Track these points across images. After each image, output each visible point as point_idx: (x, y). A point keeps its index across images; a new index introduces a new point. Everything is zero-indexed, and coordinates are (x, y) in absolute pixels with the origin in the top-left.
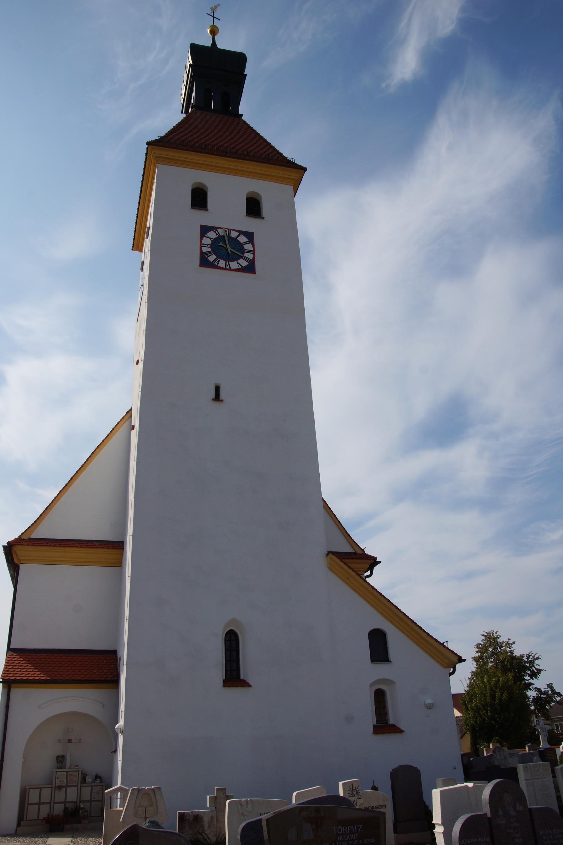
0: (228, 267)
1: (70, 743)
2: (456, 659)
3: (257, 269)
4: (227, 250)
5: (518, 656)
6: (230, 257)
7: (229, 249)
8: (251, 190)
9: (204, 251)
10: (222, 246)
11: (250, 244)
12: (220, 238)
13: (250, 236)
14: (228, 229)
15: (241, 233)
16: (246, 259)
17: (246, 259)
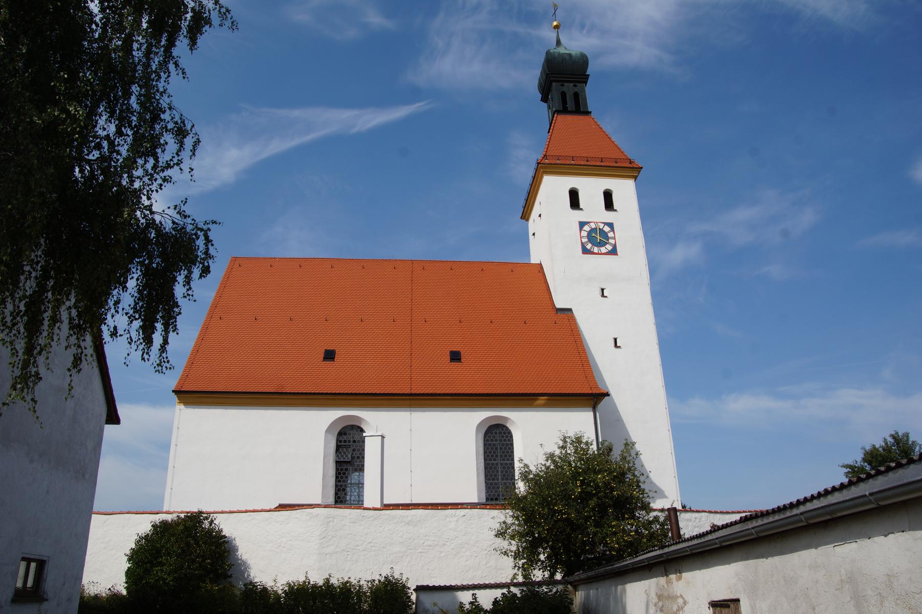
5: (491, 607)
6: (601, 244)
12: (593, 230)
13: (611, 225)
15: (605, 224)
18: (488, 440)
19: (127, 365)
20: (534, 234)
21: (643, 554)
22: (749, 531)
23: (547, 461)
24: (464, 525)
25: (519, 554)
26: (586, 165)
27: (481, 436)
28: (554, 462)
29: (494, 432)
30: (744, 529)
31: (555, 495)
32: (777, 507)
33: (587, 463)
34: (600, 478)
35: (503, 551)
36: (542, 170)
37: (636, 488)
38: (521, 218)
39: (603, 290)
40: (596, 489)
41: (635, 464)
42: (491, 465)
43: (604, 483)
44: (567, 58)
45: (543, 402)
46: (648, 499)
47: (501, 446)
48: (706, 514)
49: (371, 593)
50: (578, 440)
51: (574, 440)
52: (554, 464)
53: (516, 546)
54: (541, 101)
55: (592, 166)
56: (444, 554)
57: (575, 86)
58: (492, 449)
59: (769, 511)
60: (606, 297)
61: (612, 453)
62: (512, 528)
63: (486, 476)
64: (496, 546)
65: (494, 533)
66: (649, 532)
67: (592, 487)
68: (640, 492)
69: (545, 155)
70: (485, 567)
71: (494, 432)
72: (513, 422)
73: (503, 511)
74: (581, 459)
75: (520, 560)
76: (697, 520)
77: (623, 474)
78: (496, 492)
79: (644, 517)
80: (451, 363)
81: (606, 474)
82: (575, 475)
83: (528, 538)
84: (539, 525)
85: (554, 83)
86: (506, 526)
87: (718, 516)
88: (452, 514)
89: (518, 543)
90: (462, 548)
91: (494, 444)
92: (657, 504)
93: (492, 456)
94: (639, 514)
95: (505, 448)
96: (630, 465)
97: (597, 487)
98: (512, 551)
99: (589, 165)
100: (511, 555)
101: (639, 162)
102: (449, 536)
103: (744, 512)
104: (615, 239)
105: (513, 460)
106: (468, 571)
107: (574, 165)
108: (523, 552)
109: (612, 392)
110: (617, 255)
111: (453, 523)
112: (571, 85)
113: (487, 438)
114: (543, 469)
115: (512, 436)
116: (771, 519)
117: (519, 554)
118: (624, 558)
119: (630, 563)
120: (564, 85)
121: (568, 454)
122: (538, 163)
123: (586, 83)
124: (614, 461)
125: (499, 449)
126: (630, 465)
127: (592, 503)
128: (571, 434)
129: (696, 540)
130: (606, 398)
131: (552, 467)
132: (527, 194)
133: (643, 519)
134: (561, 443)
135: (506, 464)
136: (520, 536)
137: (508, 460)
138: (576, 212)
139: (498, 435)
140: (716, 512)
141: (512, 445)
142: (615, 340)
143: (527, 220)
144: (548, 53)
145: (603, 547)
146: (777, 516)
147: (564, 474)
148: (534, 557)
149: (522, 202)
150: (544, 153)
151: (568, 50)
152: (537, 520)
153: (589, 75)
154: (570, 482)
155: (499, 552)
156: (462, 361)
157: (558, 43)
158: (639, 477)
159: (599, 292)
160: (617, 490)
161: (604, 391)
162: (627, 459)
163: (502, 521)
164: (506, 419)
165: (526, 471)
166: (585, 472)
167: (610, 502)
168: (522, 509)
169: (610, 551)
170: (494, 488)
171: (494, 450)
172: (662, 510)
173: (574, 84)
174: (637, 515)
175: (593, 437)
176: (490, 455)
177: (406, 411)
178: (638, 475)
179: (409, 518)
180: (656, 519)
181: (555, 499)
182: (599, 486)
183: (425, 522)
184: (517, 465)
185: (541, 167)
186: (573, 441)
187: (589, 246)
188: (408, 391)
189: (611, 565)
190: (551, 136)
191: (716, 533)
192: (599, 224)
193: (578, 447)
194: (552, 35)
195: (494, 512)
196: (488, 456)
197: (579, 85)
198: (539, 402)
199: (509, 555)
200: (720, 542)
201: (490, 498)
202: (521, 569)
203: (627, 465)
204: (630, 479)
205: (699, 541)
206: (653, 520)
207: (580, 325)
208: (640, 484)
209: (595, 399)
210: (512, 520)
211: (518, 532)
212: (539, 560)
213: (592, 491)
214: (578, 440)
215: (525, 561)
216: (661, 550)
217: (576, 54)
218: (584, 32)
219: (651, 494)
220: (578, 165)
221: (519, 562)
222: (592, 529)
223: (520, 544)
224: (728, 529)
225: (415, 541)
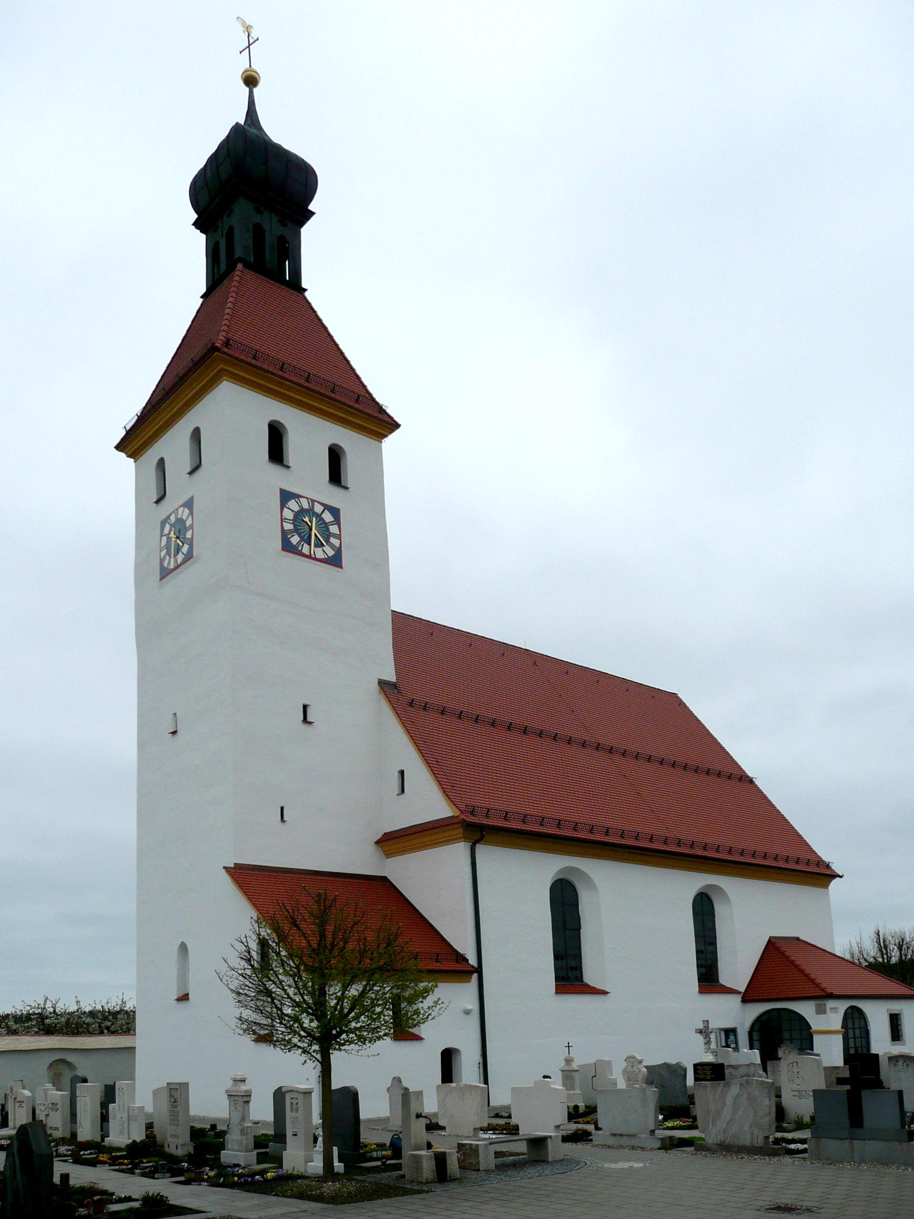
0: (313, 556)
1: (497, 1150)
2: (770, 944)
3: (344, 563)
4: (311, 529)
7: (314, 531)
8: (332, 442)
9: (285, 529)
10: (306, 522)
11: (336, 526)
14: (312, 500)
15: (327, 507)
16: (332, 546)
17: (332, 546)
19: (76, 997)
49: (352, 998)
110: (341, 567)
138: (275, 469)
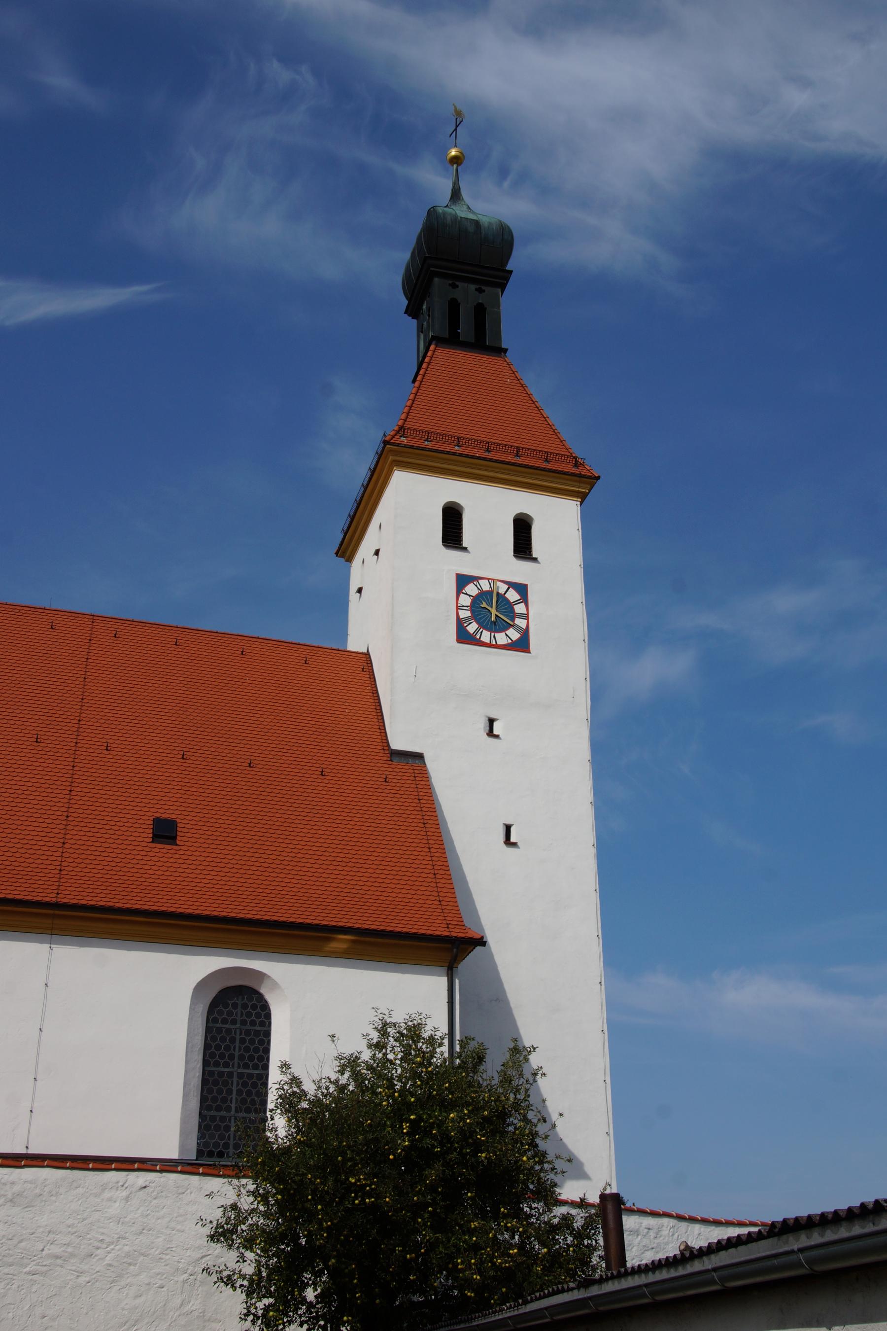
6: (498, 626)
12: (484, 596)
13: (522, 589)
15: (511, 585)
16: (518, 628)
17: (518, 628)
18: (215, 1020)
20: (360, 591)
21: (541, 1298)
22: (793, 1257)
23: (343, 1074)
24: (142, 1209)
25: (258, 1285)
26: (485, 459)
27: (202, 1009)
28: (356, 1076)
29: (230, 1002)
30: (781, 1250)
31: (353, 1151)
32: (858, 1205)
33: (427, 1083)
34: (453, 1118)
35: (225, 1274)
36: (391, 458)
37: (529, 1150)
38: (337, 554)
39: (491, 721)
40: (442, 1145)
41: (529, 1096)
42: (216, 1077)
43: (461, 1131)
44: (471, 229)
45: (344, 946)
46: (551, 1176)
47: (243, 1036)
48: (672, 1222)
50: (414, 1032)
51: (405, 1032)
52: (355, 1081)
53: (254, 1265)
54: (405, 313)
55: (496, 461)
56: (87, 1279)
57: (480, 291)
58: (223, 1039)
59: (855, 1211)
60: (497, 737)
61: (482, 1068)
62: (250, 1221)
63: (203, 1099)
64: (209, 1261)
65: (207, 1230)
66: (549, 1251)
67: (434, 1137)
68: (537, 1159)
69: (402, 428)
70: (177, 1313)
71: (230, 1002)
72: (275, 985)
73: (235, 1181)
74: (415, 1075)
75: (260, 1299)
76: (652, 1234)
77: (503, 1115)
78: (222, 1137)
79: (540, 1214)
80: (153, 845)
81: (466, 1112)
82: (400, 1110)
83: (283, 1247)
84: (311, 1216)
85: (436, 280)
86: (238, 1216)
87: (697, 1228)
88: (118, 1182)
89: (260, 1256)
90: (130, 1264)
91: (228, 1031)
92: (570, 1190)
93: (222, 1056)
94: (531, 1208)
95: (252, 1042)
96: (518, 1096)
97: (445, 1139)
98: (243, 1277)
99: (491, 460)
100: (241, 1286)
101: (593, 466)
102: (103, 1234)
103: (753, 1224)
104: (528, 619)
105: (266, 1067)
106: (137, 1321)
107: (461, 455)
108: (269, 1279)
109: (490, 938)
110: (529, 652)
111: (117, 1204)
112: (472, 287)
113: (215, 1015)
114: (331, 1090)
115: (268, 1016)
116: (843, 1232)
117: (258, 1285)
118: (491, 1307)
119: (509, 1318)
120: (457, 286)
121: (388, 1060)
122: (386, 443)
123: (503, 287)
124: (485, 1084)
125: (237, 1041)
126: (518, 1096)
127: (432, 1174)
128: (399, 1017)
129: (664, 1271)
130: (479, 949)
131: (351, 1088)
132: (356, 505)
133: (537, 1219)
134: (375, 1036)
135: (250, 1076)
136: (265, 1242)
137: (256, 1067)
139: (239, 1009)
140: (692, 1220)
141: (268, 1034)
142: (508, 828)
143: (350, 559)
144: (432, 213)
145: (447, 1279)
146: (857, 1227)
147: (377, 1105)
148: (292, 1293)
149: (342, 522)
150: (400, 423)
151: (474, 213)
152: (308, 1205)
153: (511, 272)
154: (388, 1123)
155: (214, 1278)
156: (178, 842)
157: (456, 195)
158: (536, 1126)
159: (483, 725)
160: (488, 1151)
161: (474, 933)
162: (515, 1083)
163: (229, 1202)
164: (261, 976)
165: (294, 1093)
166: (424, 1102)
167: (470, 1175)
168: (278, 1179)
169: (461, 1289)
170: (218, 1128)
171: (228, 1042)
172: (582, 1204)
173: (477, 287)
174: (526, 1209)
175: (444, 1029)
176: (217, 1053)
177: (41, 942)
178: (535, 1121)
179: (17, 1188)
180: (567, 1220)
181: (350, 1159)
182: (449, 1138)
183: (54, 1198)
184: (275, 1076)
185: (391, 450)
186: (402, 1035)
187: (472, 628)
188: (50, 898)
189: (465, 1321)
190: (419, 388)
191: (713, 1256)
192: (499, 584)
193: (410, 1046)
194: (445, 186)
195: (215, 1184)
196: (212, 1055)
197: (488, 290)
198: (334, 945)
199: (238, 1285)
200: (723, 1279)
201: (206, 1150)
202: (259, 1322)
203: (512, 1096)
204: (516, 1129)
205: (673, 1273)
206: (559, 1223)
207: (434, 784)
208: (538, 1141)
209: (455, 950)
210: (252, 1203)
211: (264, 1231)
212: (304, 1300)
213: (434, 1147)
214: (414, 1032)
215: (271, 1300)
216: (582, 1290)
217: (490, 223)
218: (506, 184)
219: (560, 1165)
220: (467, 456)
221: (258, 1304)
222: (424, 1236)
223: (263, 1260)
224: (742, 1249)
225: (23, 1244)
